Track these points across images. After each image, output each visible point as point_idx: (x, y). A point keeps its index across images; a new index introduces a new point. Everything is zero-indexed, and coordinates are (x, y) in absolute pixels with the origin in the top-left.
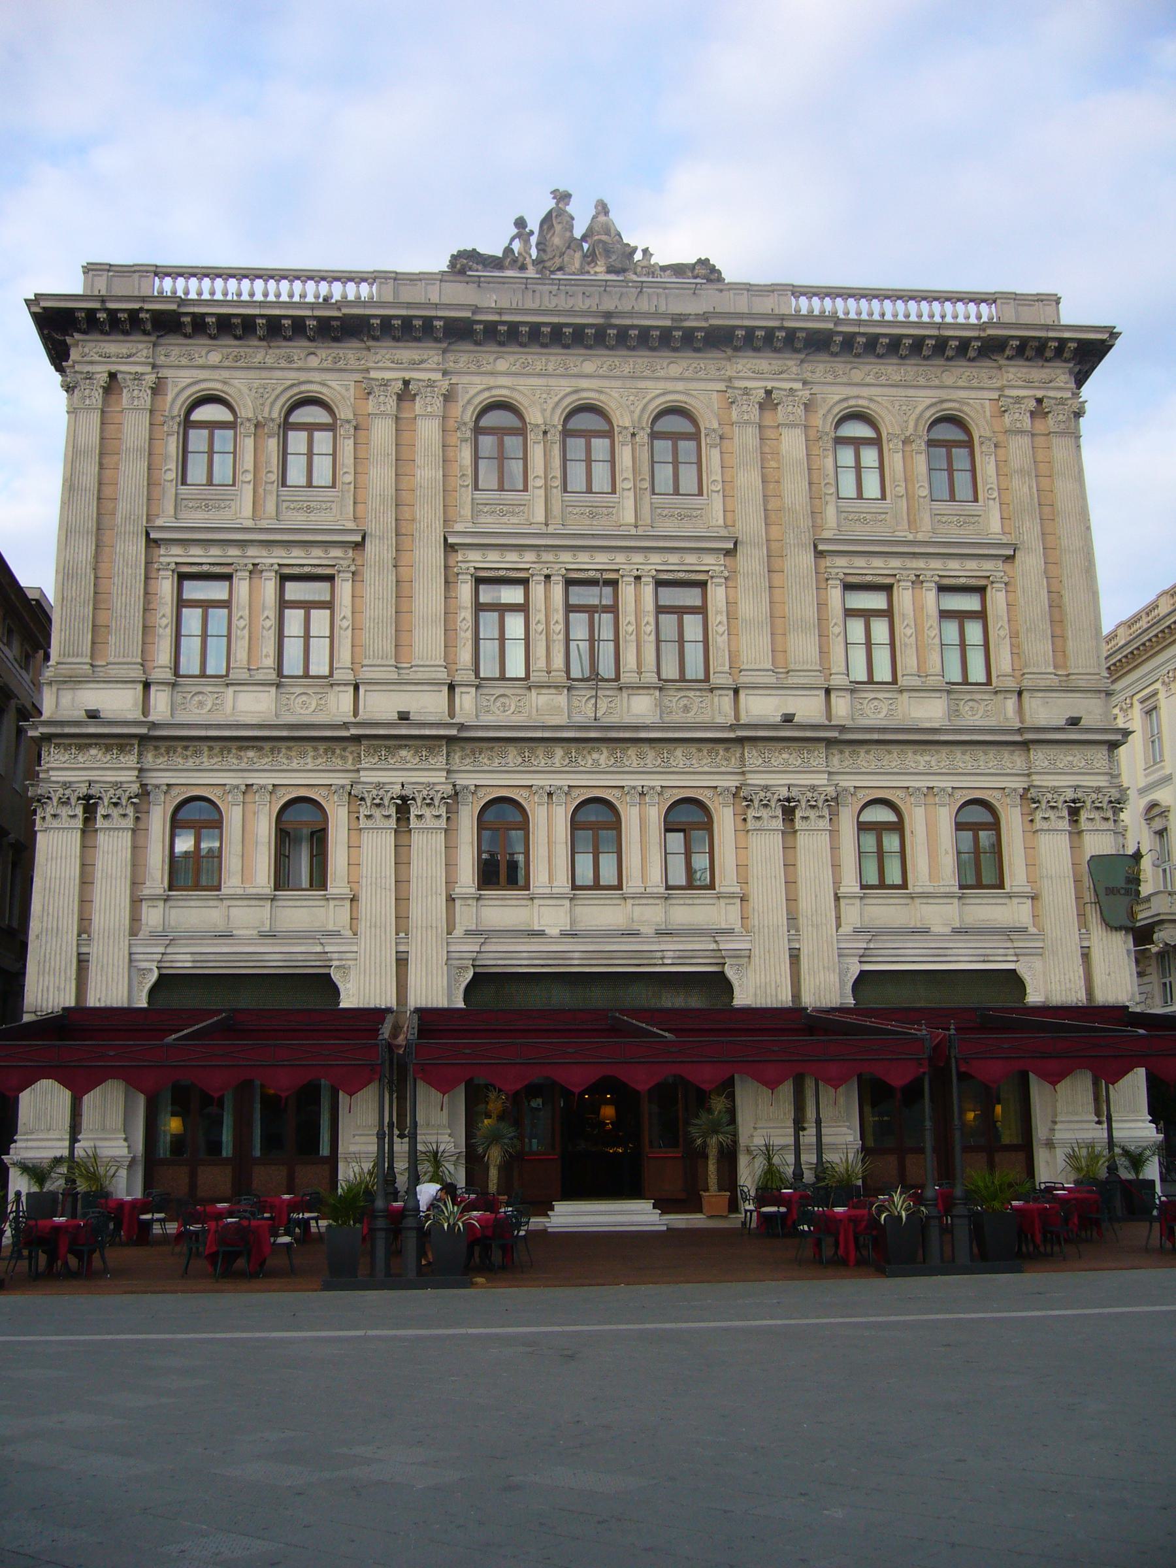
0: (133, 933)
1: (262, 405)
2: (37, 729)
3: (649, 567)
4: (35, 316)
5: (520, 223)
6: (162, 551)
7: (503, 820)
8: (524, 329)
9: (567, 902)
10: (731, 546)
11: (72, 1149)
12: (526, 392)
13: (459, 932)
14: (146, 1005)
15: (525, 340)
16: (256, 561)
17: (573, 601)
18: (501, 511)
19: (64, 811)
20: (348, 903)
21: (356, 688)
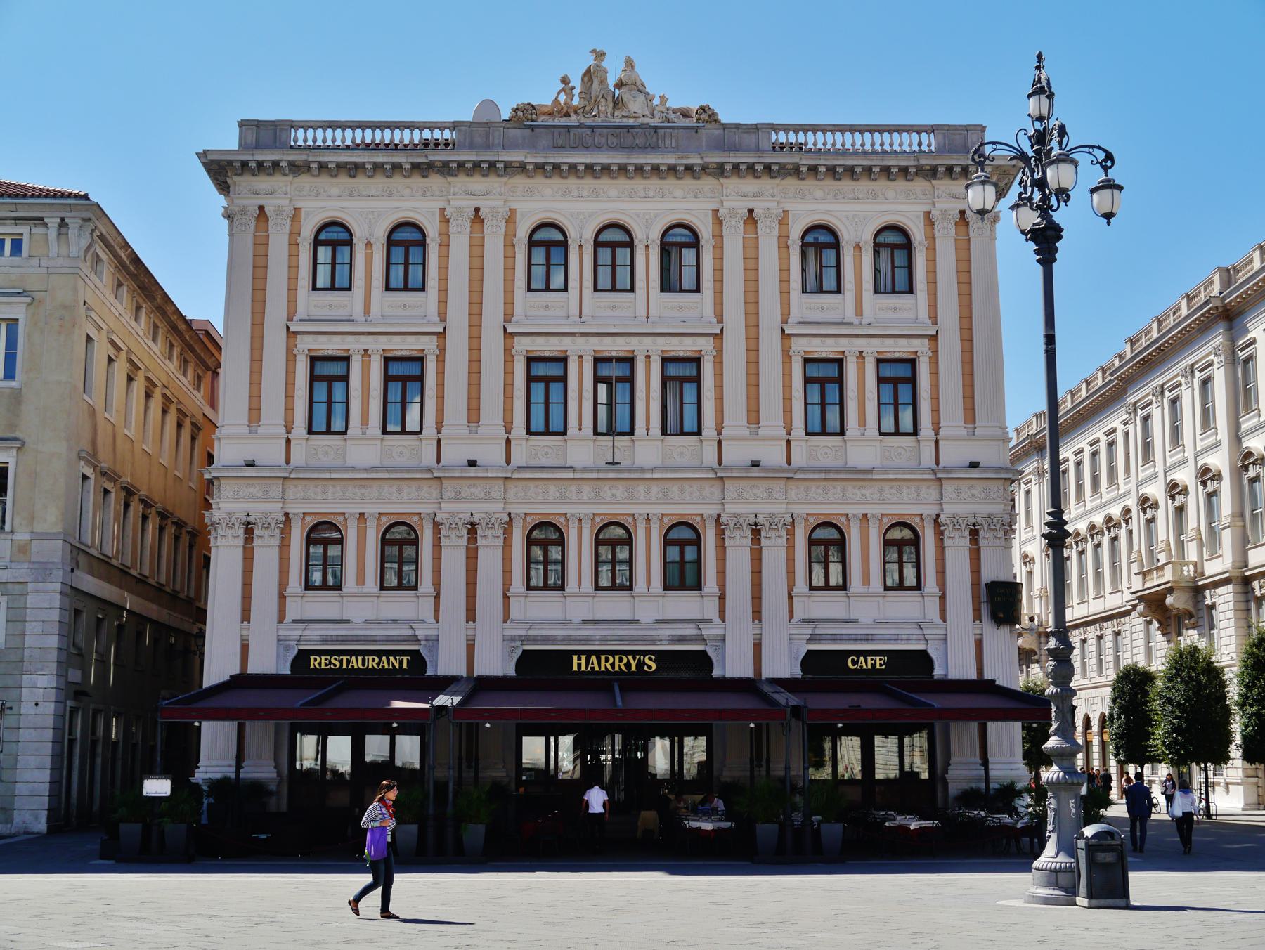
0: (281, 621)
4: (204, 164)
5: (565, 80)
11: (238, 772)
13: (288, 619)
14: (289, 672)
17: (534, 373)
19: (230, 532)
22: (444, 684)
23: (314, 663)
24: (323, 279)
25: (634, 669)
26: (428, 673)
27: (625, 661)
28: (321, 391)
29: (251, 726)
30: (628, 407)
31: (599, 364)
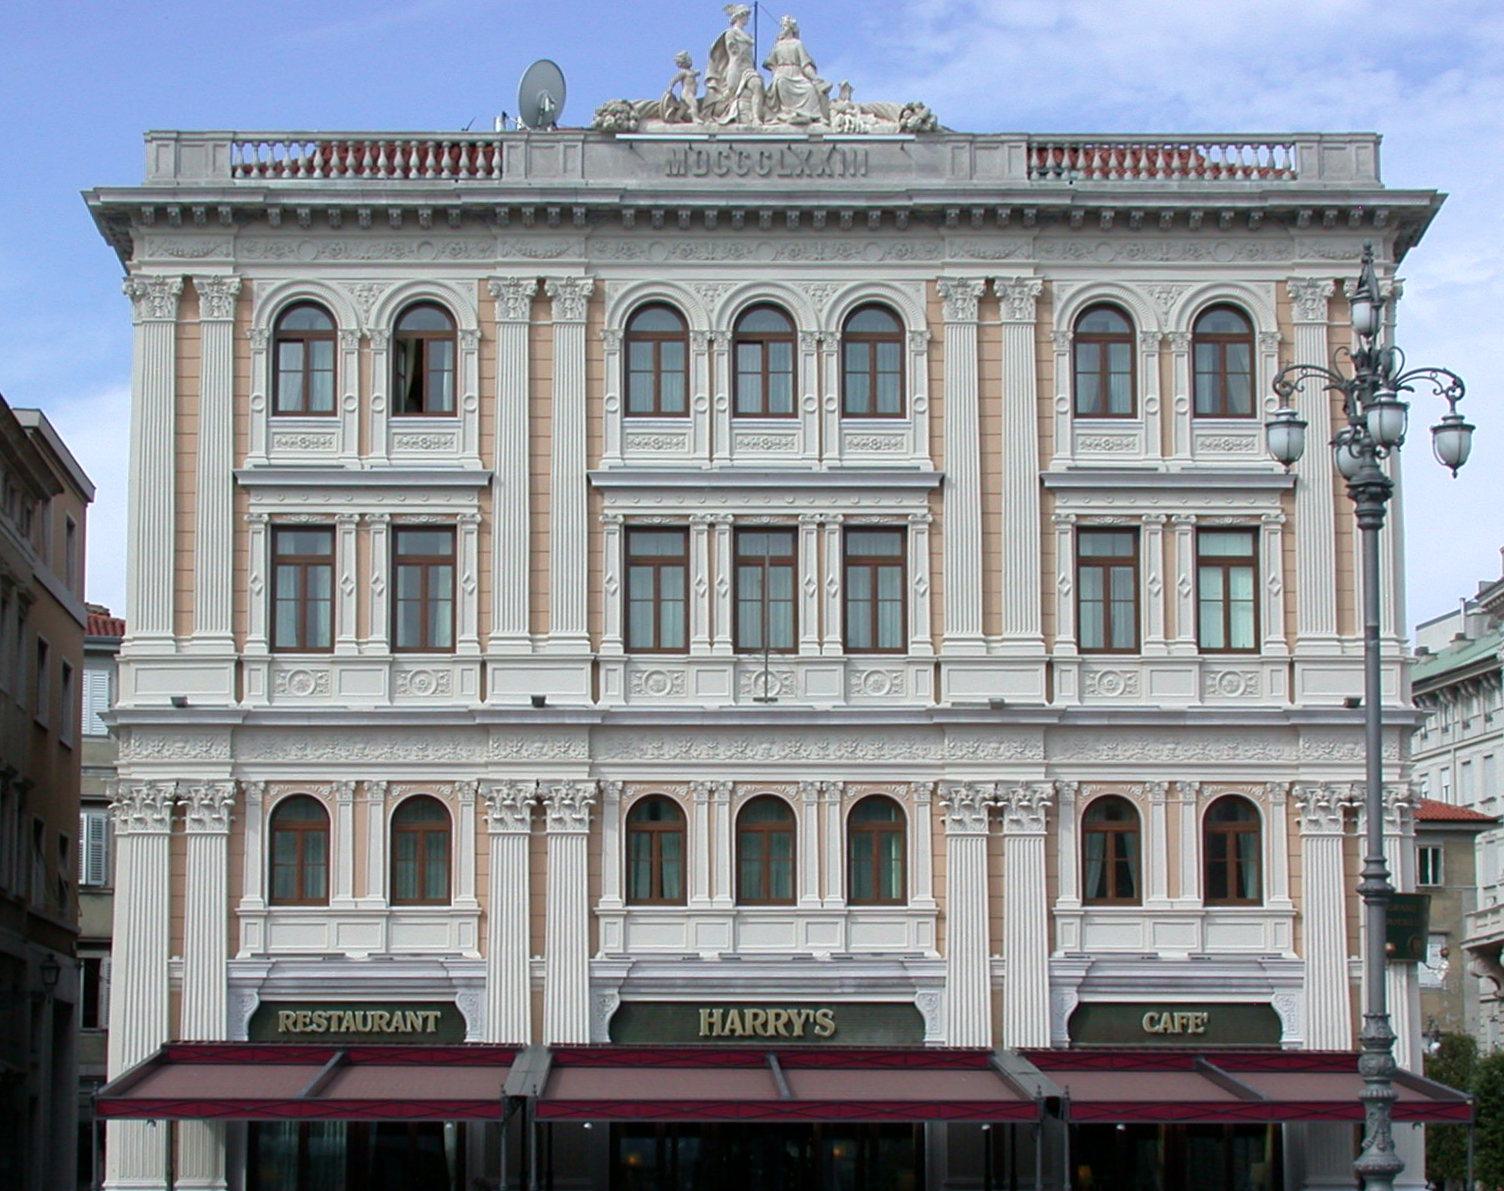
1: (367, 311)
2: (474, 718)
3: (836, 511)
4: (92, 209)
6: (607, 503)
7: (655, 823)
8: (554, 211)
9: (842, 921)
10: (1291, 485)
12: (795, 288)
15: (766, 224)
16: (1170, 512)
17: (635, 551)
18: (765, 442)
20: (475, 921)
21: (937, 666)
22: (502, 1056)
23: (285, 1020)
24: (289, 397)
25: (798, 1031)
26: (469, 1039)
27: (784, 1019)
28: (288, 577)
29: (185, 1127)
30: (898, 606)
31: (742, 536)
